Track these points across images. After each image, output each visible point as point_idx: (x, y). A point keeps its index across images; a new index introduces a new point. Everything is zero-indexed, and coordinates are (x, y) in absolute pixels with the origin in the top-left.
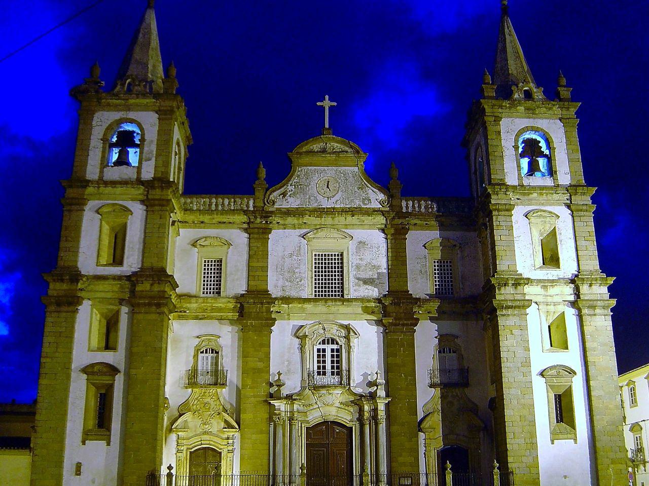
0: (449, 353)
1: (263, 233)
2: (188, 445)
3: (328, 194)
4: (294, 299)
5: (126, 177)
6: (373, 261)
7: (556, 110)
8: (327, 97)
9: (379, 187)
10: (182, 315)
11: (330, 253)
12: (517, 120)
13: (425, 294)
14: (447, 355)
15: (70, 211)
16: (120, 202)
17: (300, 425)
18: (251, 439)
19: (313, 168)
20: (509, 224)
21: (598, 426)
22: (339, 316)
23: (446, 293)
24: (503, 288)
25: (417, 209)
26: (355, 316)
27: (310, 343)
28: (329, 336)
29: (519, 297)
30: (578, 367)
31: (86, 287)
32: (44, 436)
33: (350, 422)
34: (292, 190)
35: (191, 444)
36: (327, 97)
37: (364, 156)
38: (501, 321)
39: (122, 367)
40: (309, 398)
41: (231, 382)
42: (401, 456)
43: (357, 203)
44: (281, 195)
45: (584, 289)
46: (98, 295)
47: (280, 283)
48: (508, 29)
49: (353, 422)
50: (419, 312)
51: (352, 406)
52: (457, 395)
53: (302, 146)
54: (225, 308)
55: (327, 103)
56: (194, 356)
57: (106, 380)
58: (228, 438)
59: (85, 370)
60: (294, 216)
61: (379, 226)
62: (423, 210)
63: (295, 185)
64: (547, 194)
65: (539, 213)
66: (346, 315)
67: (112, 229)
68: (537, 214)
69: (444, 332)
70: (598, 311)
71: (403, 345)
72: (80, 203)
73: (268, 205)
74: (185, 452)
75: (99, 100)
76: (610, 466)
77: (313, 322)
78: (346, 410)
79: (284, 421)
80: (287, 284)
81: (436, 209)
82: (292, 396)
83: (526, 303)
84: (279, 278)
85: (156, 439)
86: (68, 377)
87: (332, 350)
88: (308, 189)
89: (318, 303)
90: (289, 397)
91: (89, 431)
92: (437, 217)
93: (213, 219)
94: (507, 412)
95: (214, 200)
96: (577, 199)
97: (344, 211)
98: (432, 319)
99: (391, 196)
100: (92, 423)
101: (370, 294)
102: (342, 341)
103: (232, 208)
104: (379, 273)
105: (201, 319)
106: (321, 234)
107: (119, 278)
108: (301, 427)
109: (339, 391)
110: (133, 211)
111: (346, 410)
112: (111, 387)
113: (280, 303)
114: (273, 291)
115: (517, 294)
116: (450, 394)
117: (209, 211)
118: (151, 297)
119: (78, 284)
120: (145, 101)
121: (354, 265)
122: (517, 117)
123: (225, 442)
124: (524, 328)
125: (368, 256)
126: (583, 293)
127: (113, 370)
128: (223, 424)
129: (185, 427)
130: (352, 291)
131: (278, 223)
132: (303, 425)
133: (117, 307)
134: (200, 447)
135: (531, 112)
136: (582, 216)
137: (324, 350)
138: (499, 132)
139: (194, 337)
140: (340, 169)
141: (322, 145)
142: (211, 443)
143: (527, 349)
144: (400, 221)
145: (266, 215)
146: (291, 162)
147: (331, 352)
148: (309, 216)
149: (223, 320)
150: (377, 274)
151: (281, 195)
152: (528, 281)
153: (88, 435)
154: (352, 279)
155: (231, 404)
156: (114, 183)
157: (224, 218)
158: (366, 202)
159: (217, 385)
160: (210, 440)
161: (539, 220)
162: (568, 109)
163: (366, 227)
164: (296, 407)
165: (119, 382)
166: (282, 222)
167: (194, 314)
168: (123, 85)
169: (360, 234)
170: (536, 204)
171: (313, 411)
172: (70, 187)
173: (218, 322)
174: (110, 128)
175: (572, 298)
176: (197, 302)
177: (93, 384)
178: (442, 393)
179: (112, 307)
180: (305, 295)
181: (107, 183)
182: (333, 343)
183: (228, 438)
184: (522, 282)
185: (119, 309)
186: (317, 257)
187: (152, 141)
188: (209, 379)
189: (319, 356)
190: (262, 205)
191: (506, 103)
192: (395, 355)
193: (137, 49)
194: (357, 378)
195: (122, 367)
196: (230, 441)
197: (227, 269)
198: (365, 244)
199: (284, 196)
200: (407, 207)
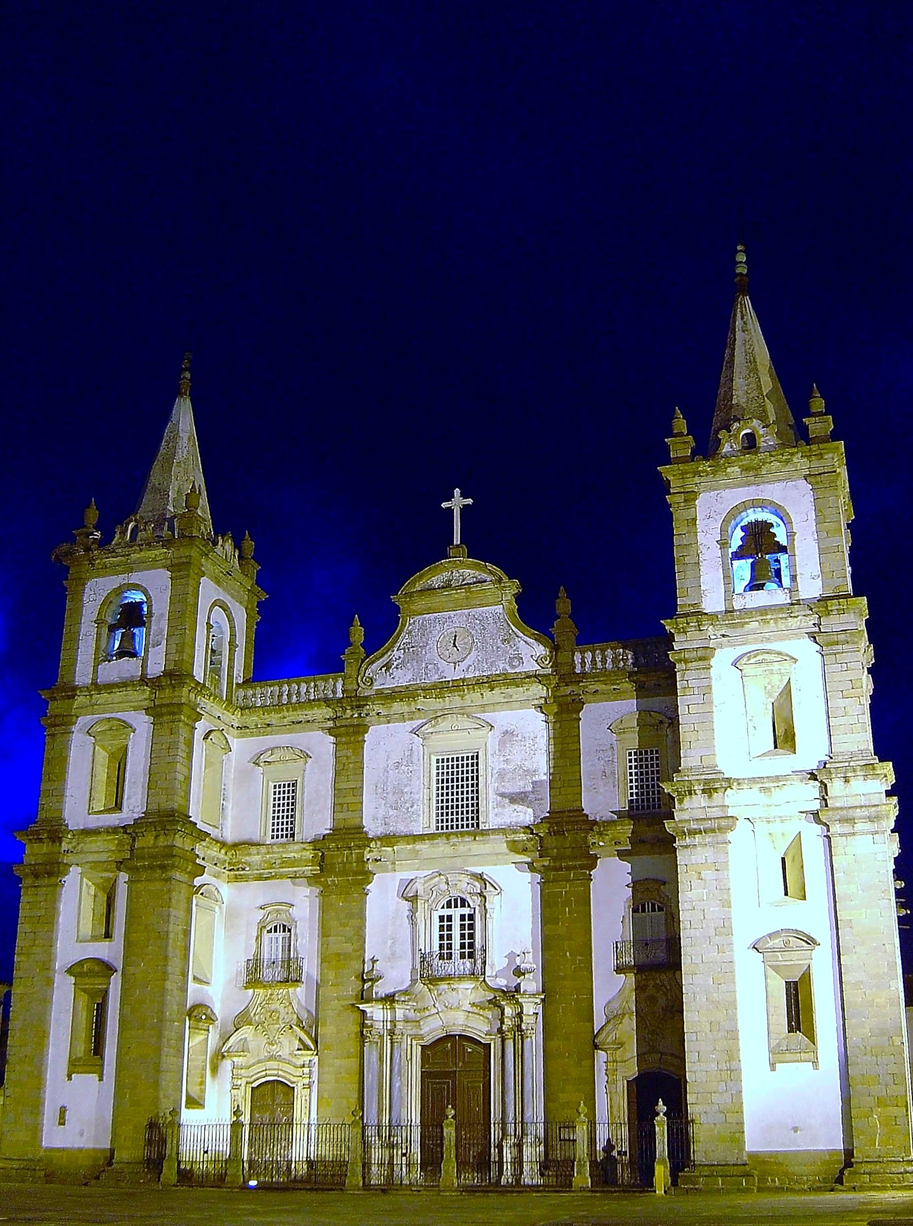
0: (652, 911)
1: (354, 733)
2: (248, 1077)
3: (455, 657)
4: (400, 837)
5: (128, 675)
6: (526, 763)
7: (800, 462)
8: (457, 491)
9: (536, 634)
10: (240, 875)
11: (460, 756)
12: (726, 494)
13: (612, 812)
14: (648, 914)
15: (53, 735)
16: (119, 715)
17: (409, 1043)
18: (333, 1065)
19: (432, 616)
20: (705, 683)
21: (852, 1039)
22: (471, 859)
23: (649, 807)
24: (687, 799)
25: (599, 665)
26: (495, 859)
27: (426, 907)
28: (455, 893)
29: (715, 812)
30: (823, 933)
31: (74, 848)
32: (18, 1068)
33: (486, 1035)
34: (400, 657)
35: (252, 1076)
36: (457, 491)
37: (513, 587)
38: (682, 857)
39: (119, 965)
40: (423, 998)
41: (309, 976)
42: (563, 1091)
43: (501, 666)
44: (383, 667)
45: (836, 787)
46: (92, 858)
47: (381, 812)
48: (742, 318)
49: (490, 1035)
50: (598, 843)
51: (489, 1009)
52: (663, 985)
53: (414, 582)
54: (300, 860)
55: (457, 502)
56: (257, 938)
57: (97, 983)
58: (303, 1066)
59: (70, 971)
60: (401, 700)
61: (536, 702)
62: (609, 665)
63: (404, 649)
64: (776, 620)
65: (760, 658)
66: (483, 858)
67: (112, 755)
68: (757, 659)
69: (643, 875)
70: (859, 826)
71: (567, 903)
72: (66, 722)
73: (364, 687)
74: (243, 1088)
75: (91, 561)
76: (874, 1110)
77: (431, 871)
78: (481, 1015)
79: (381, 1037)
80: (391, 813)
81: (631, 661)
82: (394, 996)
83: (723, 823)
84: (380, 805)
85: (158, 1070)
86: (50, 982)
87: (463, 918)
88: (424, 653)
89: (436, 841)
90: (390, 999)
91: (79, 1059)
92: (631, 674)
93: (284, 718)
94: (688, 1016)
95: (286, 688)
96: (833, 623)
97: (479, 683)
98: (622, 855)
99: (555, 648)
100: (81, 1049)
101: (521, 819)
102: (474, 901)
103: (312, 698)
104: (534, 783)
105: (266, 879)
106: (444, 725)
107: (114, 830)
108: (411, 1045)
109: (469, 985)
110: (134, 725)
111: (481, 1015)
112: (106, 992)
113: (378, 846)
114: (371, 827)
115: (710, 807)
116: (651, 983)
117: (278, 706)
118: (154, 857)
119: (60, 844)
120: (152, 554)
121: (495, 771)
122: (727, 487)
123: (299, 1072)
124: (720, 867)
125: (517, 755)
126: (833, 795)
127: (107, 968)
128: (297, 1044)
129: (244, 1049)
130: (491, 815)
131: (378, 714)
132: (414, 1042)
133: (113, 874)
134: (264, 1080)
135: (753, 473)
136: (838, 653)
137: (450, 918)
138: (695, 520)
139: (257, 907)
140: (473, 611)
141: (445, 575)
142: (280, 1073)
143: (727, 904)
144: (568, 690)
145: (357, 701)
146: (397, 609)
147: (461, 921)
148: (424, 697)
149: (298, 878)
150: (532, 783)
151: (383, 667)
152: (729, 783)
153: (75, 1065)
154: (492, 796)
155: (308, 1011)
156: (110, 687)
157: (293, 716)
158: (515, 663)
159: (288, 982)
160: (278, 1069)
161: (760, 670)
162: (821, 456)
163: (514, 705)
164: (400, 1014)
165: (115, 984)
166: (384, 712)
167: (256, 872)
168: (123, 533)
169: (503, 718)
170: (756, 641)
171: (431, 1018)
172: (54, 699)
173: (290, 883)
174: (107, 602)
175: (816, 805)
176: (258, 854)
177: (84, 990)
178: (637, 982)
179: (106, 874)
180: (418, 829)
181: (110, 687)
182: (463, 906)
183: (303, 1066)
184: (717, 785)
185: (117, 876)
186: (440, 764)
187: (162, 615)
188: (279, 973)
189: (441, 928)
190: (355, 687)
191: (705, 466)
192: (555, 921)
193: (156, 467)
194: (497, 961)
195: (119, 965)
196: (306, 1070)
197: (304, 795)
198: (513, 735)
199: (388, 669)
200: (583, 663)
